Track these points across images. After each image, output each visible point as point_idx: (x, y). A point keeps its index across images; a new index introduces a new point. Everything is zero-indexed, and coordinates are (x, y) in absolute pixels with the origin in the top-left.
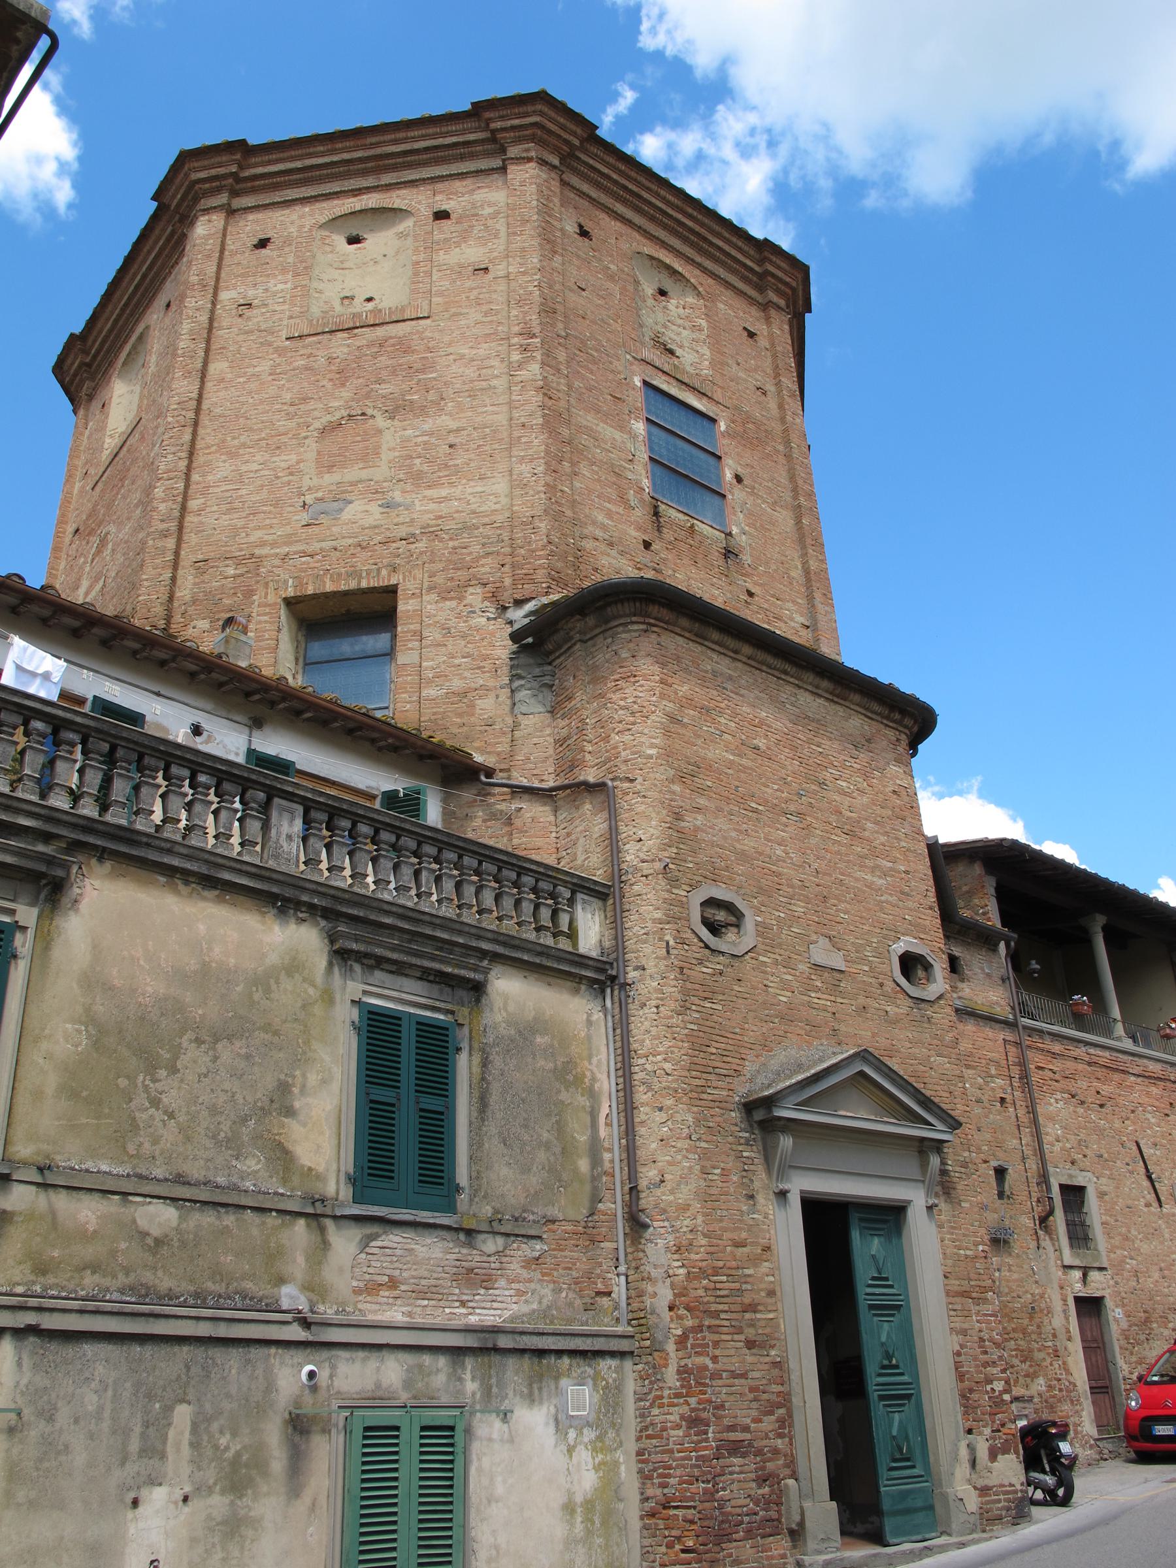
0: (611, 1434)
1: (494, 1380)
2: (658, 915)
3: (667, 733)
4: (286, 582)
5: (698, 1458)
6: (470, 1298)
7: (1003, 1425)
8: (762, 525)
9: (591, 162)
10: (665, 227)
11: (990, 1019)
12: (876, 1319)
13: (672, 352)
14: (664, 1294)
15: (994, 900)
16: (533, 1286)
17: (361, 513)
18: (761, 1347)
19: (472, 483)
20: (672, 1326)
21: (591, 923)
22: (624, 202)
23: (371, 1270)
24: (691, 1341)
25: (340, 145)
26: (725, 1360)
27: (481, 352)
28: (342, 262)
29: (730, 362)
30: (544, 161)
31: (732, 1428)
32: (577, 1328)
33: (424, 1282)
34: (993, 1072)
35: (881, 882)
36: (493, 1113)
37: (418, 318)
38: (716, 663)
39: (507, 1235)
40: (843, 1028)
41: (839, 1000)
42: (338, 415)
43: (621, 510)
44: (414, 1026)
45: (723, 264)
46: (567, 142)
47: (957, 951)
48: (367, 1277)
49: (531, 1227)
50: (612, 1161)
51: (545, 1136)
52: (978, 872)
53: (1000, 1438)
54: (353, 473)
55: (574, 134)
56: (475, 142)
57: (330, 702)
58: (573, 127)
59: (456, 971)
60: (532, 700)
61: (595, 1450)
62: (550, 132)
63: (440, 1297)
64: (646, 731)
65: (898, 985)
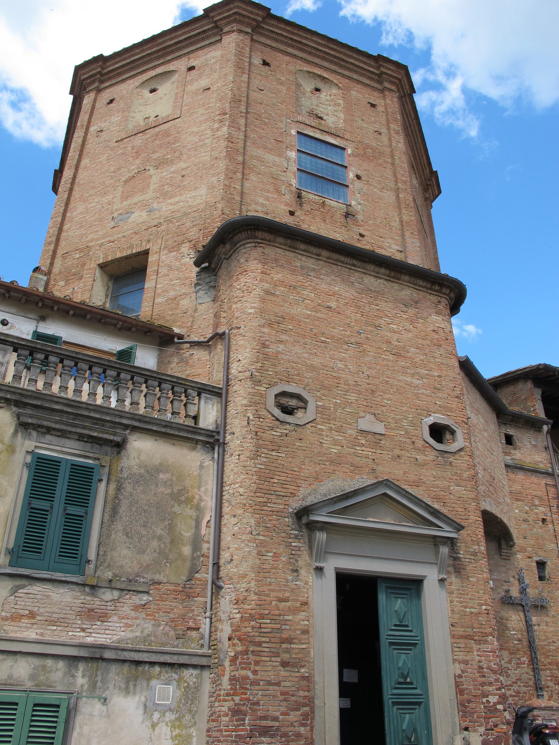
0: (188, 717)
1: (99, 678)
2: (245, 402)
3: (263, 300)
4: (100, 256)
5: (236, 736)
6: (88, 627)
7: (496, 726)
8: (372, 200)
9: (271, 28)
10: (318, 57)
11: (535, 471)
12: (395, 651)
13: (321, 118)
14: (225, 630)
15: (540, 403)
16: (138, 621)
17: (139, 217)
18: (294, 666)
19: (190, 192)
20: (229, 650)
21: (211, 411)
22: (292, 46)
23: (16, 607)
24: (239, 660)
25: (145, 47)
26: (263, 673)
27: (202, 128)
28: (146, 102)
29: (357, 119)
30: (241, 31)
31: (265, 718)
32: (166, 649)
33: (54, 615)
34: (537, 502)
35: (419, 382)
36: (121, 517)
37: (175, 119)
38: (302, 261)
39: (122, 590)
40: (380, 468)
41: (379, 451)
42: (133, 173)
43: (276, 196)
44: (69, 466)
45: (356, 72)
46: (254, 20)
47: (511, 432)
48: (13, 610)
49: (140, 586)
50: (209, 549)
51: (159, 532)
52: (530, 386)
53: (492, 734)
54: (137, 198)
55: (258, 15)
56: (208, 30)
57: (80, 303)
58: (257, 12)
59: (100, 435)
60: (205, 296)
61: (173, 727)
62: (244, 16)
63: (66, 625)
64: (249, 300)
65: (427, 443)
